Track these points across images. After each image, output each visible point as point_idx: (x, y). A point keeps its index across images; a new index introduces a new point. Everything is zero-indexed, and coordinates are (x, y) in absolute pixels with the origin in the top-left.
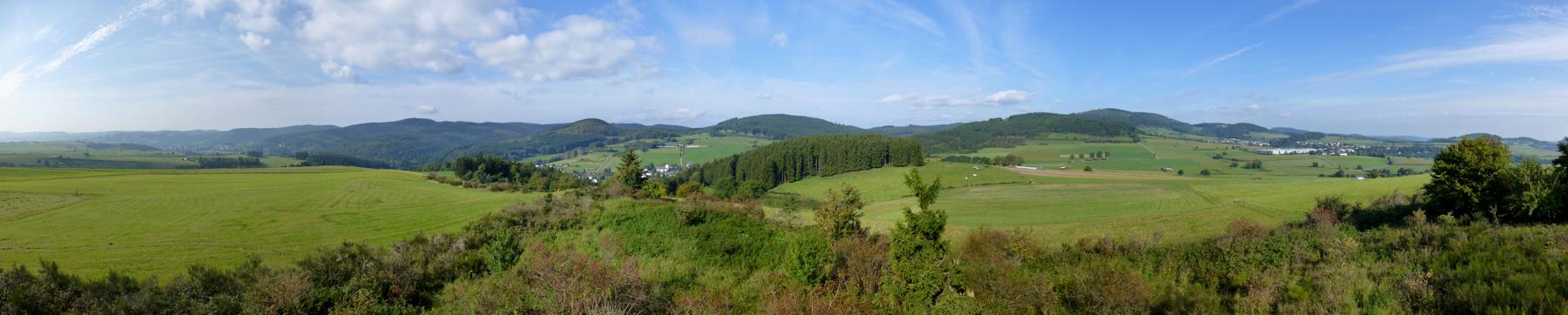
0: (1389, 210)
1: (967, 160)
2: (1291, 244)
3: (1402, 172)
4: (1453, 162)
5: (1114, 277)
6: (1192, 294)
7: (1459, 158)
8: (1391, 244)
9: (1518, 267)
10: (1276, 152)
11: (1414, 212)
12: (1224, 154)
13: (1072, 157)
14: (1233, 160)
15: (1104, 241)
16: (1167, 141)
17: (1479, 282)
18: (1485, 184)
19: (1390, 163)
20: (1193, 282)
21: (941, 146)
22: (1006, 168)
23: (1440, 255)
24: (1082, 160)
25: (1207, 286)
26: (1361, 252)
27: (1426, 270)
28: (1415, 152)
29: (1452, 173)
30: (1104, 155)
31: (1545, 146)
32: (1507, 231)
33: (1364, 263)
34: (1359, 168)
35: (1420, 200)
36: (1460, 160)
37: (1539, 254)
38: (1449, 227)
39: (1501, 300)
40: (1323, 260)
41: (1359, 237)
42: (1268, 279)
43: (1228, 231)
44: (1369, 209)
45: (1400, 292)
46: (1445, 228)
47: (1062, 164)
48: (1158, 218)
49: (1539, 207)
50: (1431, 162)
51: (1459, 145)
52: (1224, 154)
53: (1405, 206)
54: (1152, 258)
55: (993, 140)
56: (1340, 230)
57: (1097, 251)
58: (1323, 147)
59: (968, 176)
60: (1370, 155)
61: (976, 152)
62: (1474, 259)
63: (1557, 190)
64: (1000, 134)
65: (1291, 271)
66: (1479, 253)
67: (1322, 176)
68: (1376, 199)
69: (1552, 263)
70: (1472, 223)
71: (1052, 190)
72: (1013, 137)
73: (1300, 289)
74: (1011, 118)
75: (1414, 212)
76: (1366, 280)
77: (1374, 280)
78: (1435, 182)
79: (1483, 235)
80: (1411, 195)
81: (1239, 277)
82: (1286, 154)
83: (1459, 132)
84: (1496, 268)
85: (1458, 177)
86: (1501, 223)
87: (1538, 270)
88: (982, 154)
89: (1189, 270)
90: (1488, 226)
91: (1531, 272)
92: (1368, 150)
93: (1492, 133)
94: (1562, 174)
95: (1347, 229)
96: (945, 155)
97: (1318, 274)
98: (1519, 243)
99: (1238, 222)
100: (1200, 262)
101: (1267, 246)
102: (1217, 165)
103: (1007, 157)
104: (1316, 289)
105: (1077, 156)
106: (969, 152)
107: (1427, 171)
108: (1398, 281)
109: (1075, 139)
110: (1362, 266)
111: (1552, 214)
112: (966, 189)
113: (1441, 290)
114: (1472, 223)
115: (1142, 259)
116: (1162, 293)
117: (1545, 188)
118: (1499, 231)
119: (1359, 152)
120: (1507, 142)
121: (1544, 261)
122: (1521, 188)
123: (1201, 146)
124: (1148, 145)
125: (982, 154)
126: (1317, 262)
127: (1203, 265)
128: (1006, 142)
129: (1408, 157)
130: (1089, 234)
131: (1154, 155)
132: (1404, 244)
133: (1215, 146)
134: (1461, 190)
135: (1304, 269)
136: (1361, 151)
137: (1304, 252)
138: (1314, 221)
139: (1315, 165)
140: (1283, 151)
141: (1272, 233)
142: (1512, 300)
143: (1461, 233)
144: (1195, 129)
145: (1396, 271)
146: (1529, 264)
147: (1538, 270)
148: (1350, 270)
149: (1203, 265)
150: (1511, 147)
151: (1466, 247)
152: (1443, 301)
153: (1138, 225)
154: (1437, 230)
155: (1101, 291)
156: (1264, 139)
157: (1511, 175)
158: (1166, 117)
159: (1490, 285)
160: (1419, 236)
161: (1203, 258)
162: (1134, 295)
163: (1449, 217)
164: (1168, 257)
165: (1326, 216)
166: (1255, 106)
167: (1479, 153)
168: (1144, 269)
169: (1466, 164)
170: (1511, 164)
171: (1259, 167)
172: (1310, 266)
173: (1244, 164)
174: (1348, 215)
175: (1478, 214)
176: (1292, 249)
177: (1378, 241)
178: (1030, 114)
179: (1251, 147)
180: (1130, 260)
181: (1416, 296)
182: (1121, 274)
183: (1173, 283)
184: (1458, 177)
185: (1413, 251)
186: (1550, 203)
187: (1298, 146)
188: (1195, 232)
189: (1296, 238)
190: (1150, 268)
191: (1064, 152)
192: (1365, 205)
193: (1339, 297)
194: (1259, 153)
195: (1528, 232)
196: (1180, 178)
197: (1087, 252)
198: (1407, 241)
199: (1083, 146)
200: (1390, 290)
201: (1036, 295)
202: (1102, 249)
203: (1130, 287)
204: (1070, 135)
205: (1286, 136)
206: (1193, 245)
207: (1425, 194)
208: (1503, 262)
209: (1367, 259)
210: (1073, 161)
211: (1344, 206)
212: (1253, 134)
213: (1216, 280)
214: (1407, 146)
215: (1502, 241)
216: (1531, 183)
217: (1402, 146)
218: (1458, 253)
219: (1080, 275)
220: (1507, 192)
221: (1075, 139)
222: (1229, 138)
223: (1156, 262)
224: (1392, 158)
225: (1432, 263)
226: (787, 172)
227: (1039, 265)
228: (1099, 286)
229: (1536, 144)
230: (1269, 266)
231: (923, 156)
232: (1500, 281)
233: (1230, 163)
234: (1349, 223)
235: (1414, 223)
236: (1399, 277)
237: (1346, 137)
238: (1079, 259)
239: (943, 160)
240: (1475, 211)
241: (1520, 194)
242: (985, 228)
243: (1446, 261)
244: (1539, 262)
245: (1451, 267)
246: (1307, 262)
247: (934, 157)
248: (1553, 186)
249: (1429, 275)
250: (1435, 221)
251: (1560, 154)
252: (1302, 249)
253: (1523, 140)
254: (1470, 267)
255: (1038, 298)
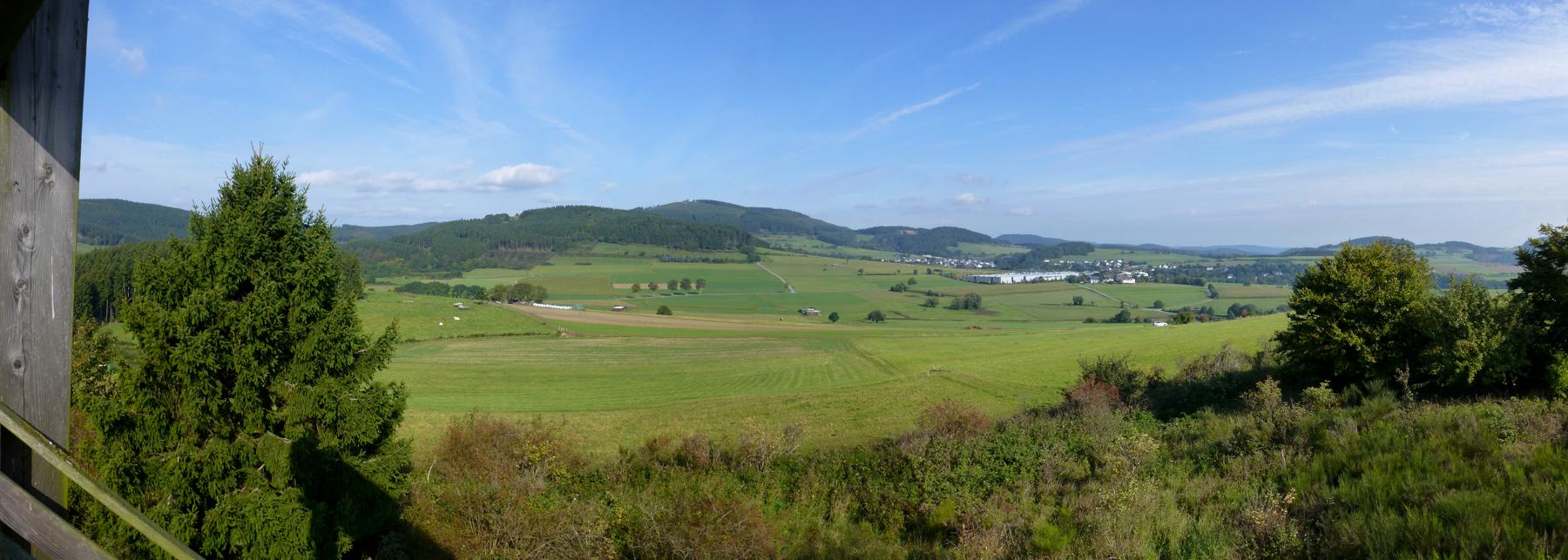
0: (1214, 381)
1: (443, 291)
2: (1035, 448)
3: (1236, 312)
4: (1328, 290)
5: (711, 510)
6: (854, 543)
7: (1340, 283)
8: (1219, 444)
9: (1452, 479)
10: (1006, 278)
11: (1259, 384)
12: (912, 282)
13: (636, 289)
14: (929, 294)
15: (690, 445)
16: (810, 258)
17: (1380, 508)
18: (1387, 328)
19: (1214, 295)
20: (856, 520)
21: (396, 262)
22: (514, 306)
23: (1310, 461)
24: (654, 295)
25: (882, 528)
26: (1164, 460)
27: (1283, 490)
28: (1258, 273)
29: (1326, 311)
30: (693, 286)
31: (1494, 257)
32: (1430, 412)
33: (1171, 480)
34: (1158, 305)
35: (1269, 361)
36: (1340, 287)
37: (1490, 454)
38: (1323, 410)
39: (1423, 541)
40: (1095, 476)
41: (1160, 433)
42: (995, 515)
43: (921, 425)
44: (1176, 381)
45: (1237, 533)
46: (1316, 412)
47: (617, 301)
48: (793, 401)
49: (1485, 369)
50: (1287, 291)
51: (1339, 260)
52: (912, 282)
53: (1249, 371)
54: (782, 475)
55: (492, 255)
56: (1126, 419)
57: (681, 461)
58: (1092, 268)
59: (444, 319)
60: (1176, 282)
61: (459, 275)
62: (1371, 467)
63: (1517, 335)
64: (504, 243)
65: (1038, 498)
66: (1380, 454)
67: (1090, 321)
68: (1189, 361)
69: (1513, 469)
70: (1365, 401)
71: (597, 349)
72: (529, 250)
73: (1053, 530)
74: (526, 213)
75: (1259, 384)
76: (1174, 512)
77: (1190, 511)
78: (1295, 327)
79: (1386, 421)
80: (1253, 353)
81: (942, 510)
82: (1025, 281)
83: (1334, 234)
84: (1410, 482)
85: (1337, 317)
86: (1418, 399)
87: (1488, 483)
88: (470, 279)
89: (849, 498)
90: (1394, 405)
91: (1476, 488)
92: (1174, 273)
93: (1397, 236)
94: (1526, 306)
95: (1138, 417)
96: (403, 281)
97: (1086, 501)
98: (1451, 436)
99: (939, 408)
100: (870, 482)
101: (992, 451)
102: (899, 302)
103: (517, 286)
104: (1085, 531)
105: (644, 286)
106: (446, 277)
107: (1281, 309)
108: (1233, 513)
109: (642, 255)
110: (1167, 486)
111: (1509, 380)
112: (440, 343)
113: (1313, 525)
114: (1365, 401)
115: (763, 476)
116: (799, 540)
117: (1495, 333)
118: (1415, 415)
119: (1157, 276)
120: (1424, 252)
121: (1498, 466)
122: (1452, 334)
123: (869, 267)
124: (774, 267)
125: (470, 279)
126: (1085, 480)
127: (874, 487)
128: (515, 259)
129: (1246, 284)
130: (667, 431)
131: (786, 287)
132: (1241, 443)
133: (892, 268)
134: (1344, 341)
135: (1061, 494)
136: (1159, 275)
137: (1061, 463)
138: (1077, 404)
139: (1078, 302)
140: (1018, 278)
141: (1001, 428)
142: (1442, 540)
143: (1347, 420)
144: (859, 238)
145: (1228, 494)
146: (1470, 473)
147: (1488, 483)
148: (1144, 492)
149: (874, 487)
150: (1431, 259)
151: (1355, 446)
152: (1316, 547)
153: (755, 413)
154: (1301, 415)
155: (687, 536)
156: (983, 255)
157: (1434, 312)
158: (806, 217)
159: (1402, 513)
160: (1269, 427)
161: (875, 475)
162: (748, 543)
163: (1323, 392)
164: (812, 474)
165: (1100, 394)
166: (968, 197)
167: (1374, 273)
168: (767, 496)
169: (1351, 294)
170: (1432, 291)
171: (975, 307)
172: (1072, 487)
173: (947, 301)
174: (1138, 393)
175: (1376, 385)
176: (1038, 456)
177: (1195, 438)
178: (560, 209)
179: (961, 271)
180: (741, 478)
181: (1266, 538)
182: (723, 503)
183: (820, 521)
184: (1337, 317)
185: (1259, 455)
186: (1506, 361)
187: (1046, 268)
188: (861, 426)
189: (1046, 437)
190: (777, 493)
191: (621, 279)
192: (1171, 373)
193: (1126, 544)
194: (975, 281)
195: (1466, 412)
196: (832, 327)
197: (664, 463)
198: (1247, 437)
199: (657, 268)
200: (1218, 529)
201: (574, 543)
202: (690, 457)
203: (741, 529)
204: (634, 249)
205: (1026, 251)
206: (856, 451)
207: (1278, 350)
208: (1424, 470)
209: (1175, 473)
210: (637, 296)
211: (1131, 376)
212: (964, 247)
213: (899, 515)
214: (1243, 263)
215: (1421, 431)
216: (1469, 324)
217: (1234, 264)
218: (1341, 456)
219: (649, 506)
220: (1426, 341)
221: (642, 255)
222: (919, 254)
223: (788, 483)
224: (1216, 285)
225: (1294, 476)
226: (115, 304)
227: (576, 487)
228: (684, 526)
229: (1476, 252)
230: (997, 488)
231: (363, 280)
232: (1420, 506)
233: (923, 299)
234: (1142, 406)
235: (1260, 404)
236: (1235, 505)
237: (1132, 249)
238: (648, 476)
239: (399, 290)
240: (1371, 379)
241: (1451, 345)
242: (479, 416)
243: (1319, 474)
244: (1488, 468)
245: (1329, 483)
246: (1066, 480)
247: (382, 283)
248: (1510, 329)
249: (1290, 498)
250: (1298, 399)
251: (1521, 270)
252: (1057, 456)
253: (1453, 247)
254: (1364, 482)
255: (577, 548)
